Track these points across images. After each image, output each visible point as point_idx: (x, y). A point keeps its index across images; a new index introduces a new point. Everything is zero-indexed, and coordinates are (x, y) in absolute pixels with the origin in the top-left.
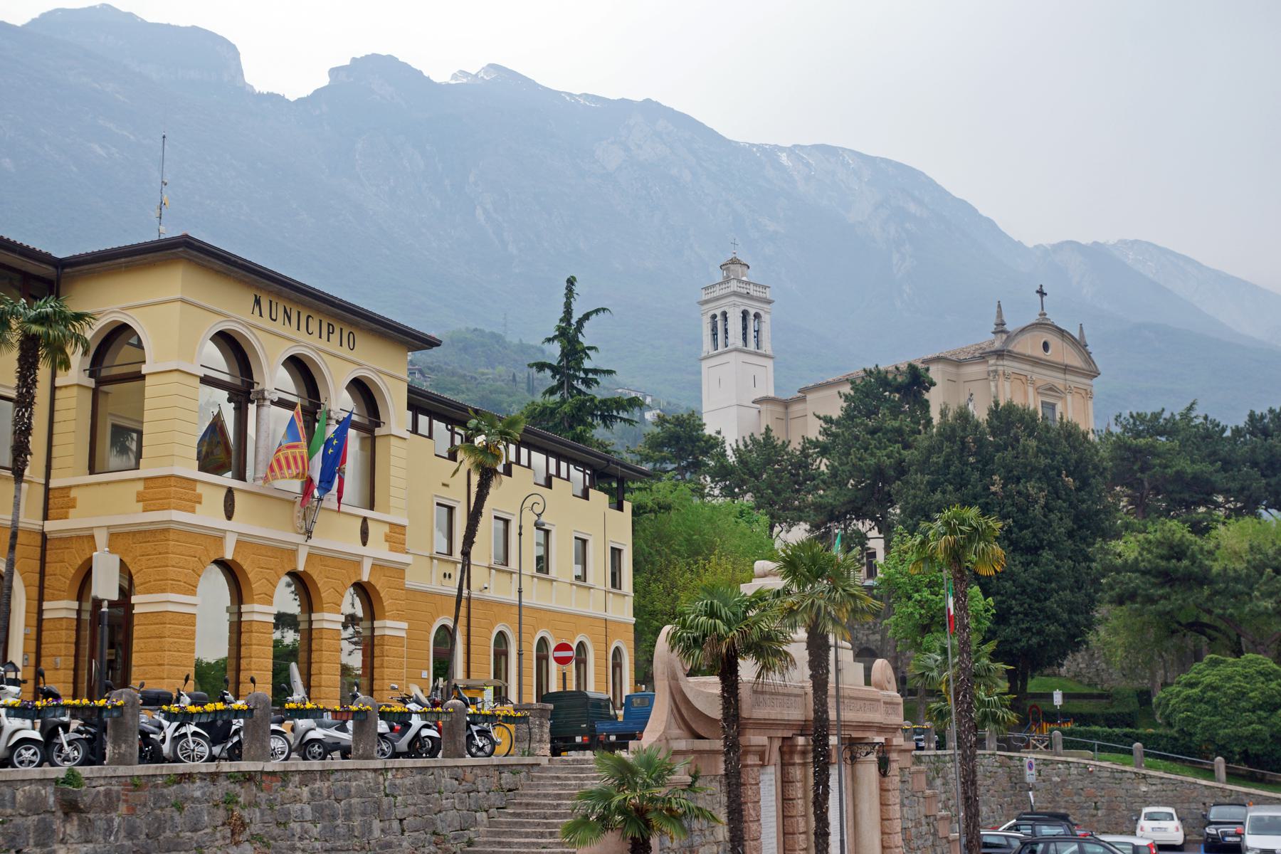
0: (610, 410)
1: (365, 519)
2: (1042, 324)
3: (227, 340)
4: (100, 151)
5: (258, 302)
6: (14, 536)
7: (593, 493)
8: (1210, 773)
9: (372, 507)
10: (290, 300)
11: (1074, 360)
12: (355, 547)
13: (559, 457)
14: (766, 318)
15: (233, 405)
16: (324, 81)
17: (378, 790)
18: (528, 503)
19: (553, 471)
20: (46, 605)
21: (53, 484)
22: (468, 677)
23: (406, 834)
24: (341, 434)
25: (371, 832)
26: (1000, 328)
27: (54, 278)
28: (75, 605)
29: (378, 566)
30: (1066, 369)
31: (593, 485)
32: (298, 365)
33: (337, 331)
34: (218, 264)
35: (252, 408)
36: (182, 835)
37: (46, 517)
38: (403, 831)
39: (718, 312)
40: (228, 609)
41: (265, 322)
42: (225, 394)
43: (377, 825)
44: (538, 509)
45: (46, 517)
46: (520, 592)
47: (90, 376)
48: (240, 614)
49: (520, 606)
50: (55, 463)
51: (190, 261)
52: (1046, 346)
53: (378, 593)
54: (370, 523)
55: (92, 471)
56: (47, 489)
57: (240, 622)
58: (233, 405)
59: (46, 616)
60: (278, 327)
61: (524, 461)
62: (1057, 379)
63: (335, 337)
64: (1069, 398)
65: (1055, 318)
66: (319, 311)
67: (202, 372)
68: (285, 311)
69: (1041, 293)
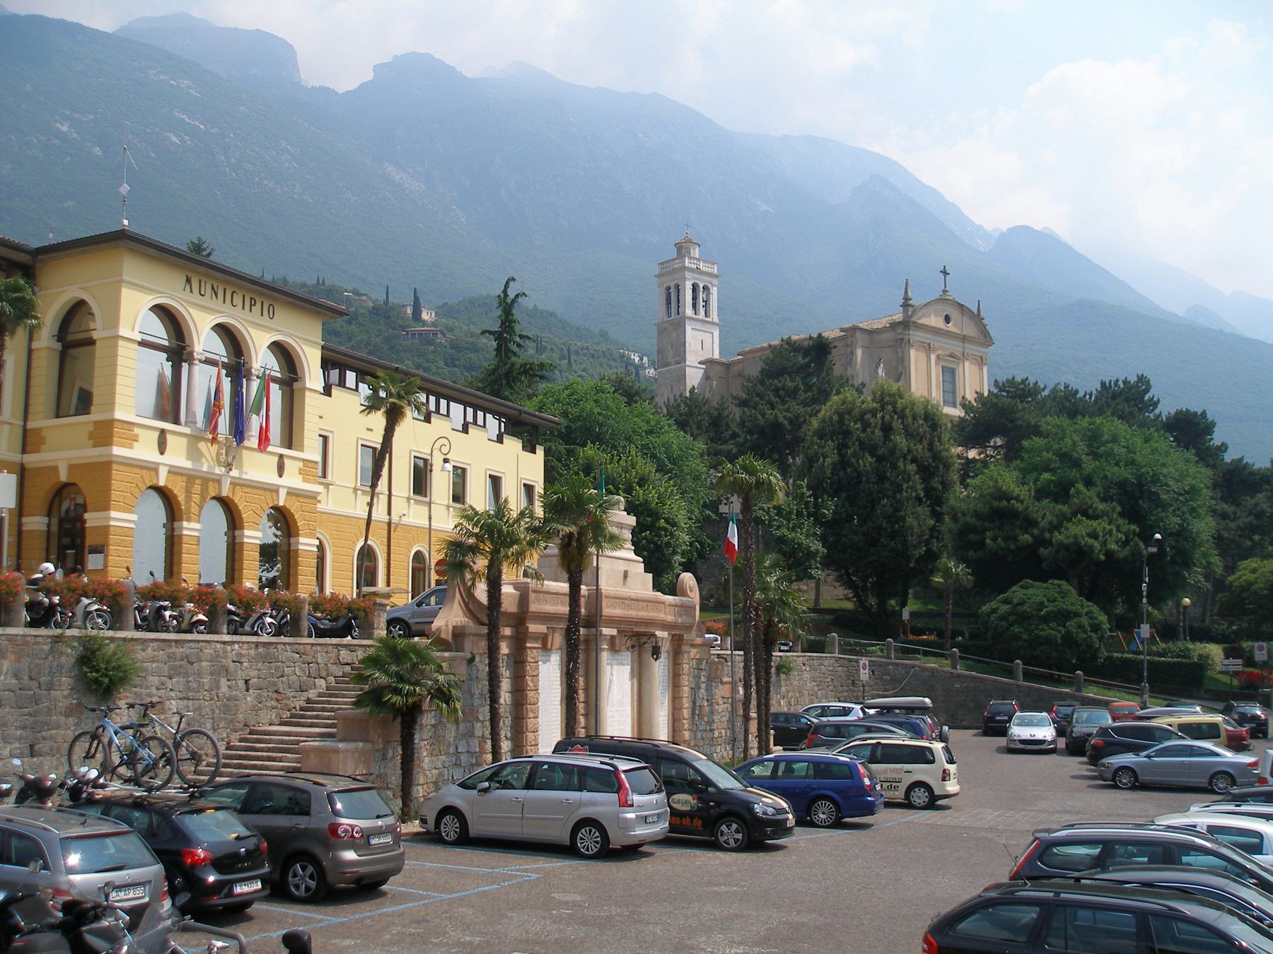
0: (534, 372)
1: (281, 456)
2: (943, 299)
3: (163, 312)
4: (174, 139)
7: (507, 439)
8: (1010, 673)
9: (290, 447)
10: (215, 279)
11: (970, 330)
12: (271, 477)
13: (476, 408)
14: (714, 291)
16: (369, 76)
17: (226, 657)
18: (437, 445)
19: (470, 419)
22: (388, 585)
24: (265, 390)
25: (218, 688)
26: (906, 304)
27: (30, 262)
28: (46, 520)
29: (292, 493)
30: (964, 339)
31: (507, 432)
32: (224, 331)
34: (153, 252)
35: (185, 366)
37: (24, 451)
39: (672, 285)
40: (164, 526)
41: (195, 297)
42: (165, 355)
43: (224, 683)
44: (445, 450)
45: (24, 451)
46: (430, 518)
48: (234, 538)
49: (389, 524)
50: (32, 409)
51: (132, 251)
52: (947, 319)
54: (286, 461)
55: (58, 416)
56: (25, 431)
59: (24, 528)
60: (206, 301)
61: (443, 410)
62: (956, 347)
63: (257, 309)
64: (967, 364)
65: (954, 294)
66: (241, 288)
67: (139, 338)
69: (945, 273)
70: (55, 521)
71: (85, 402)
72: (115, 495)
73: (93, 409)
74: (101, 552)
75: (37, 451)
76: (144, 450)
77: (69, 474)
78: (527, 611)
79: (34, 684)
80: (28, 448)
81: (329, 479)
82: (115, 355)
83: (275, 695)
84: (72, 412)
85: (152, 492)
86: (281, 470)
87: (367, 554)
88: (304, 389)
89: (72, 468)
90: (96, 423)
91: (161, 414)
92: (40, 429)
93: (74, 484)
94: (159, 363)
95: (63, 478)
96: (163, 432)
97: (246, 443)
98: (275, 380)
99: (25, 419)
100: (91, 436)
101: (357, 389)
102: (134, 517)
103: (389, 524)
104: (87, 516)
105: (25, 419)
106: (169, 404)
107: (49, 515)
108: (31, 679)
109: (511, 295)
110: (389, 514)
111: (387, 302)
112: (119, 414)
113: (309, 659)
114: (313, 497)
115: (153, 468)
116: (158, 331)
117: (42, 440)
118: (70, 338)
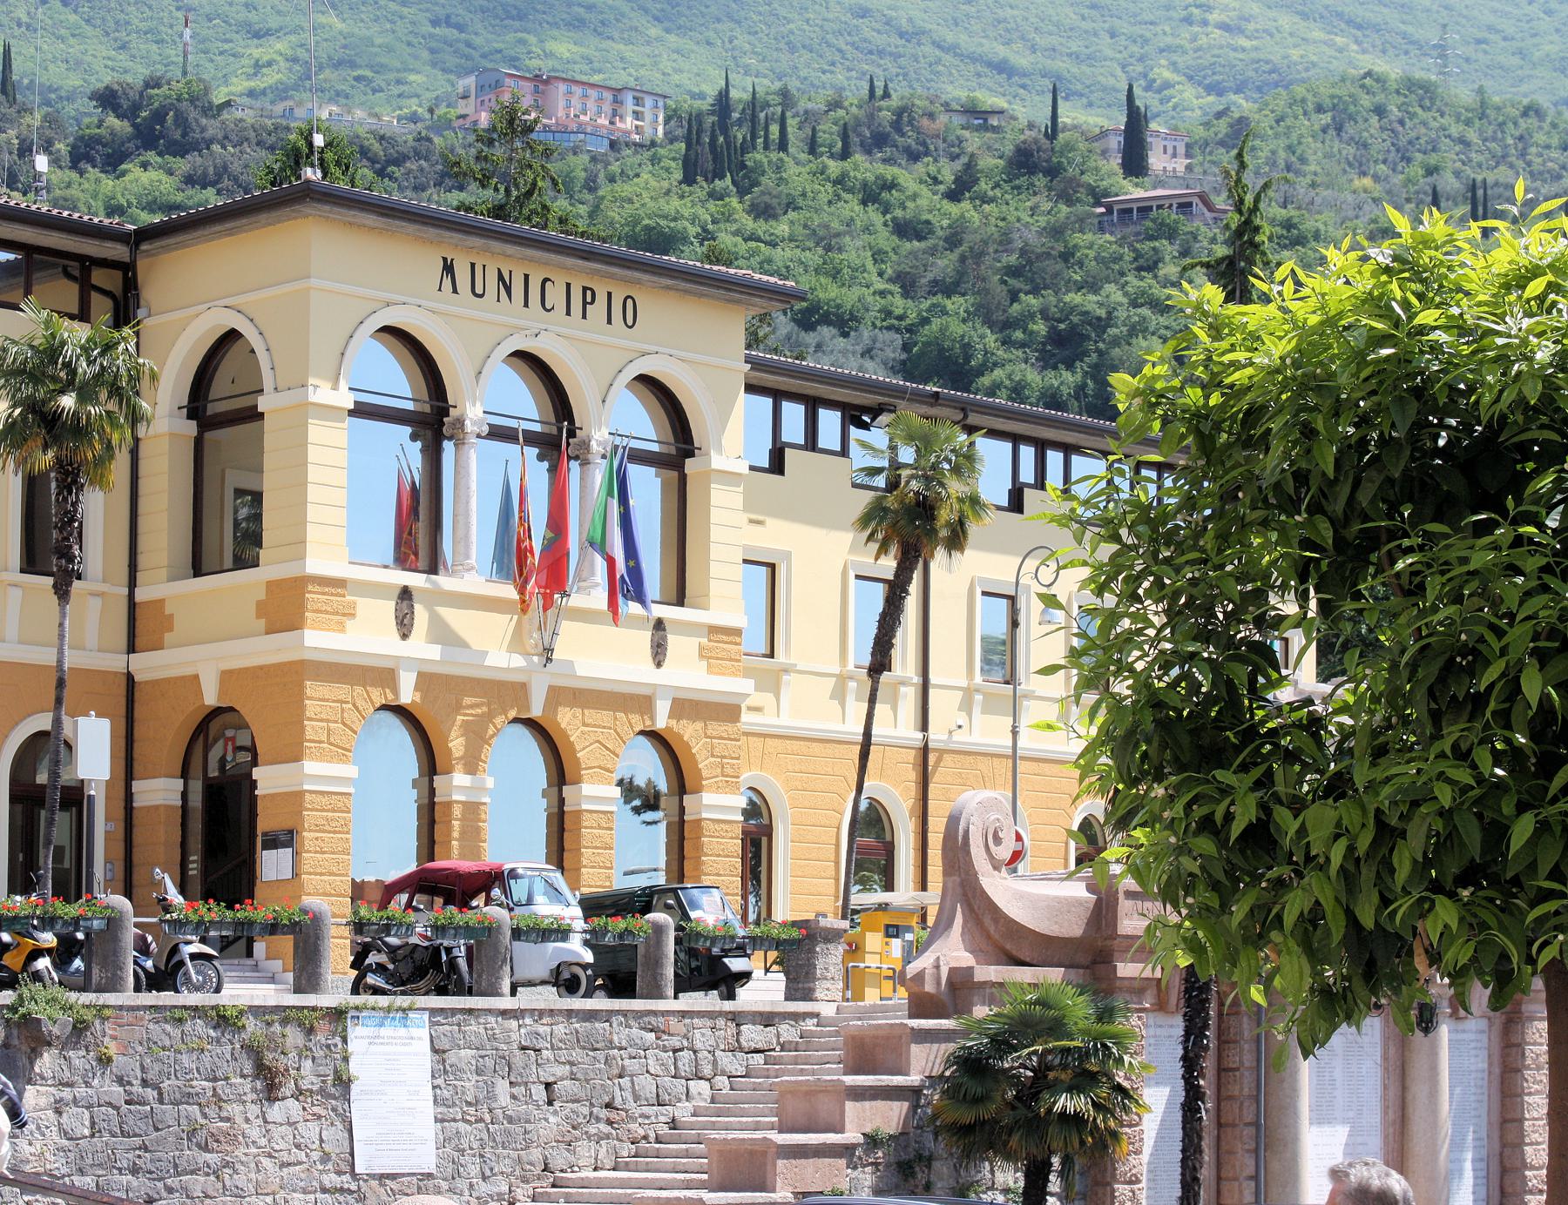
5: (448, 268)
6: (61, 683)
9: (680, 601)
15: (419, 444)
20: (137, 786)
21: (141, 595)
23: (557, 1104)
29: (685, 707)
33: (601, 299)
34: (371, 219)
35: (448, 446)
36: (195, 1083)
37: (132, 648)
38: (550, 1103)
40: (415, 783)
43: (502, 1087)
45: (132, 648)
47: (189, 417)
49: (925, 750)
50: (142, 560)
53: (688, 747)
55: (198, 571)
56: (132, 605)
57: (561, 814)
58: (419, 444)
63: (598, 310)
68: (501, 277)
70: (197, 787)
71: (247, 548)
72: (312, 729)
73: (263, 554)
74: (289, 843)
75: (158, 646)
76: (367, 633)
77: (222, 691)
78: (1114, 935)
79: (151, 1094)
80: (139, 642)
81: (781, 656)
82: (303, 444)
83: (604, 1113)
84: (228, 562)
85: (389, 717)
86: (659, 652)
87: (871, 824)
88: (708, 475)
89: (227, 677)
90: (271, 586)
91: (405, 556)
92: (160, 603)
93: (232, 709)
94: (399, 450)
95: (211, 699)
96: (406, 594)
97: (576, 600)
98: (639, 457)
99: (132, 584)
100: (262, 609)
101: (844, 452)
102: (350, 771)
103: (925, 750)
104: (257, 773)
105: (132, 584)
106: (419, 530)
107: (185, 774)
108: (145, 1083)
109: (1251, 181)
110: (924, 726)
111: (1053, 131)
112: (315, 564)
113: (675, 1042)
114: (727, 711)
115: (385, 676)
116: (396, 383)
117: (167, 623)
118: (212, 409)
